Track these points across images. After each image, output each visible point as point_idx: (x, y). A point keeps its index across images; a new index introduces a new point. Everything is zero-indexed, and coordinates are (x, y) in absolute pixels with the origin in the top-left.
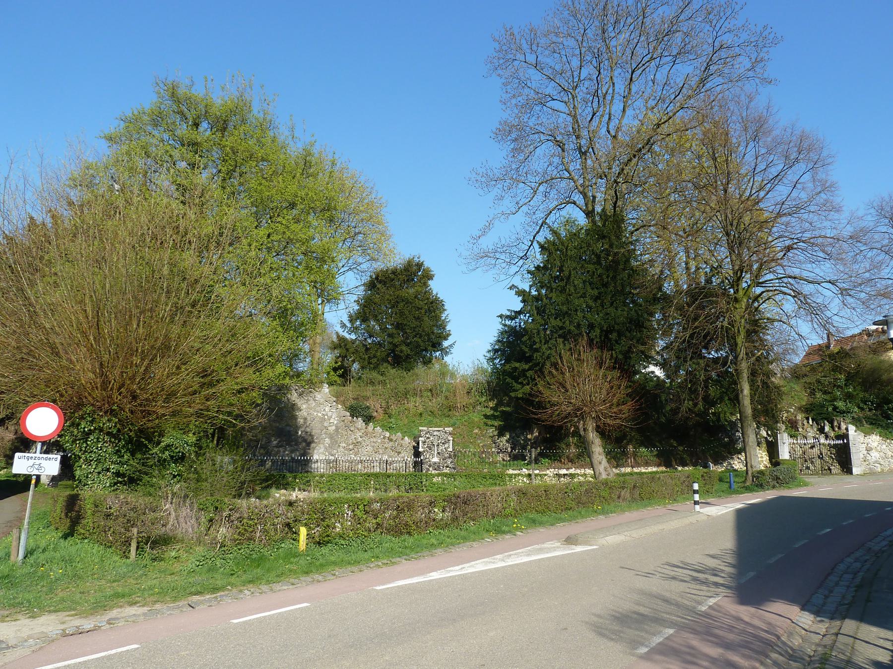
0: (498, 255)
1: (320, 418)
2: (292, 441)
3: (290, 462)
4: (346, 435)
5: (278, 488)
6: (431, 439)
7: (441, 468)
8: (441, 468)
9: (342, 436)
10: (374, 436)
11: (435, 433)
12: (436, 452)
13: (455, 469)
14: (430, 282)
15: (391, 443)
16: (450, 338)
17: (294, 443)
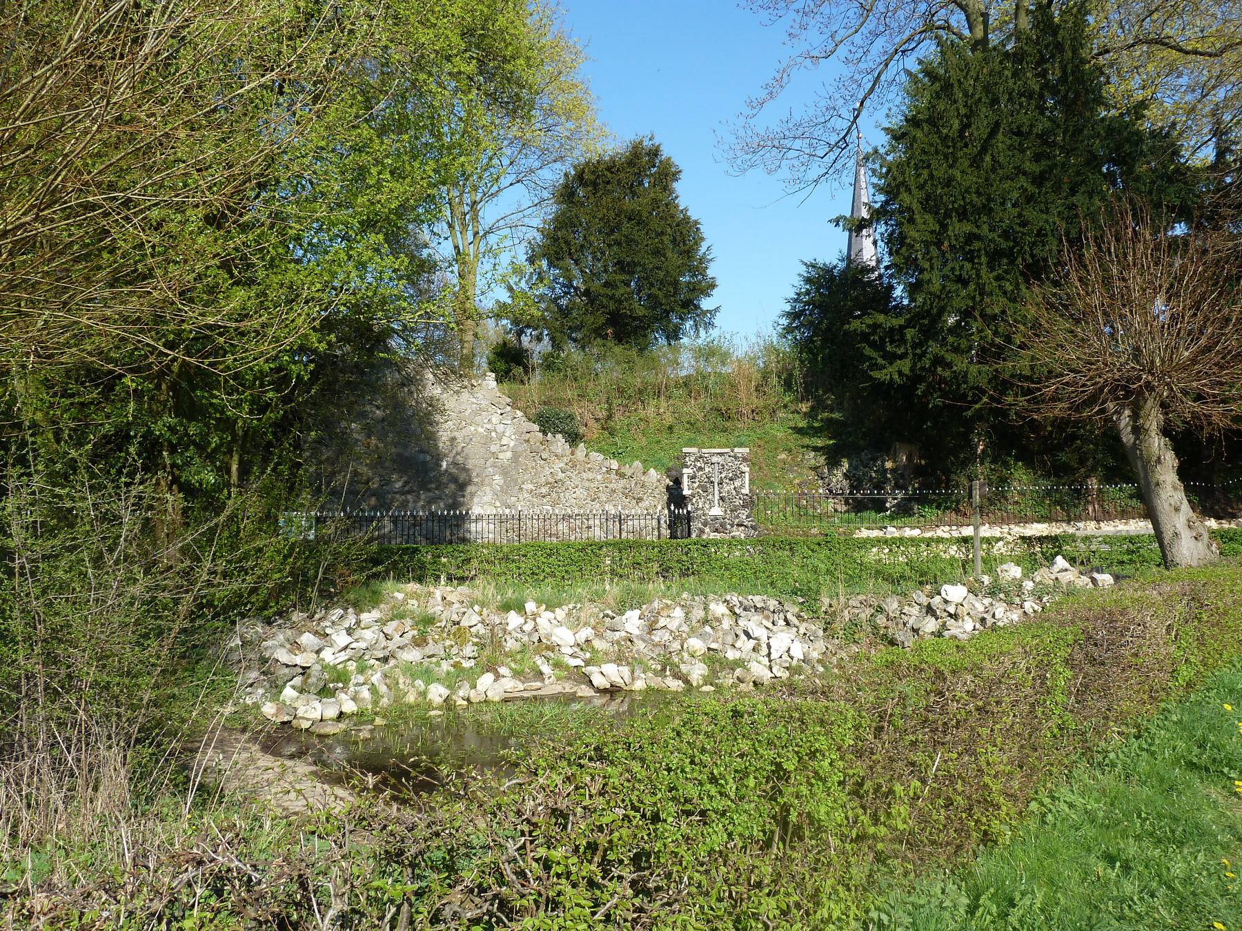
0: (787, 143)
1: (482, 437)
2: (431, 482)
3: (427, 520)
4: (532, 468)
5: (398, 578)
6: (707, 470)
7: (728, 527)
8: (728, 527)
9: (526, 470)
10: (589, 469)
11: (715, 459)
12: (717, 497)
13: (755, 530)
14: (675, 185)
15: (623, 482)
16: (714, 292)
17: (433, 486)
